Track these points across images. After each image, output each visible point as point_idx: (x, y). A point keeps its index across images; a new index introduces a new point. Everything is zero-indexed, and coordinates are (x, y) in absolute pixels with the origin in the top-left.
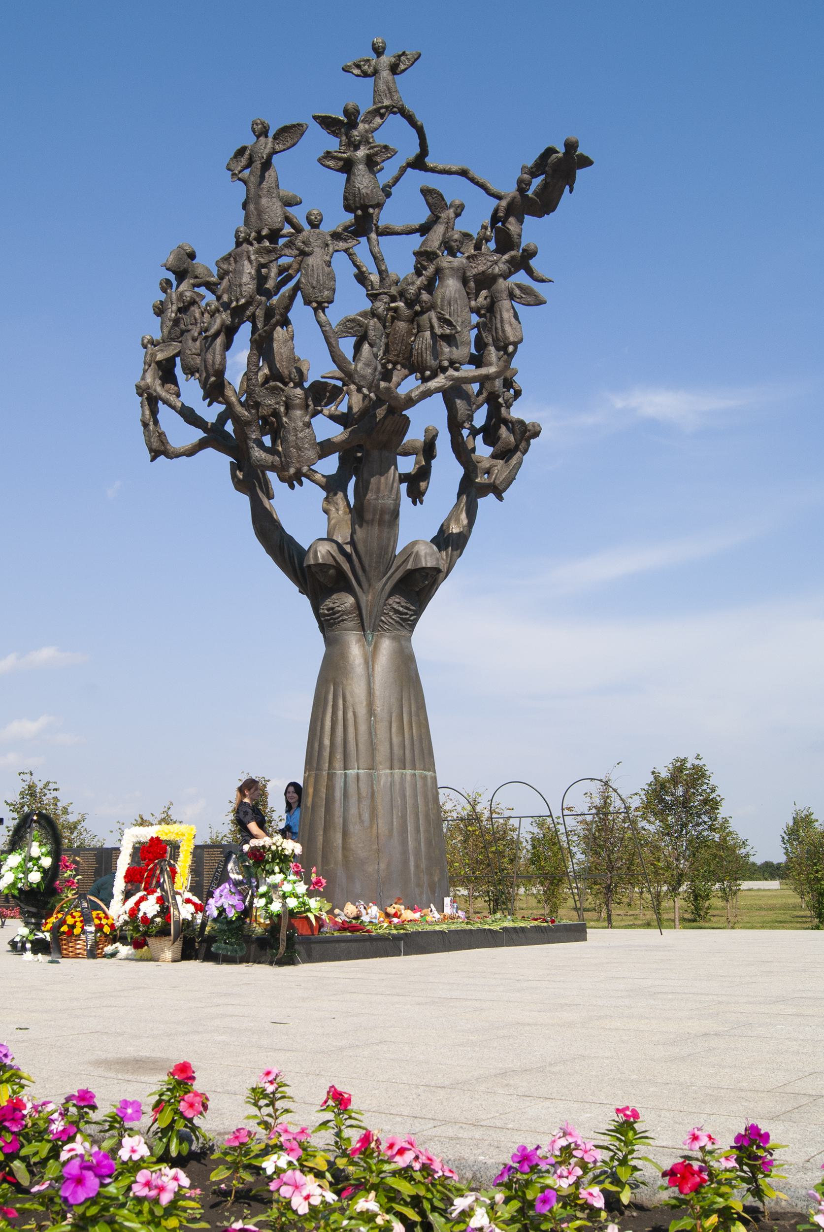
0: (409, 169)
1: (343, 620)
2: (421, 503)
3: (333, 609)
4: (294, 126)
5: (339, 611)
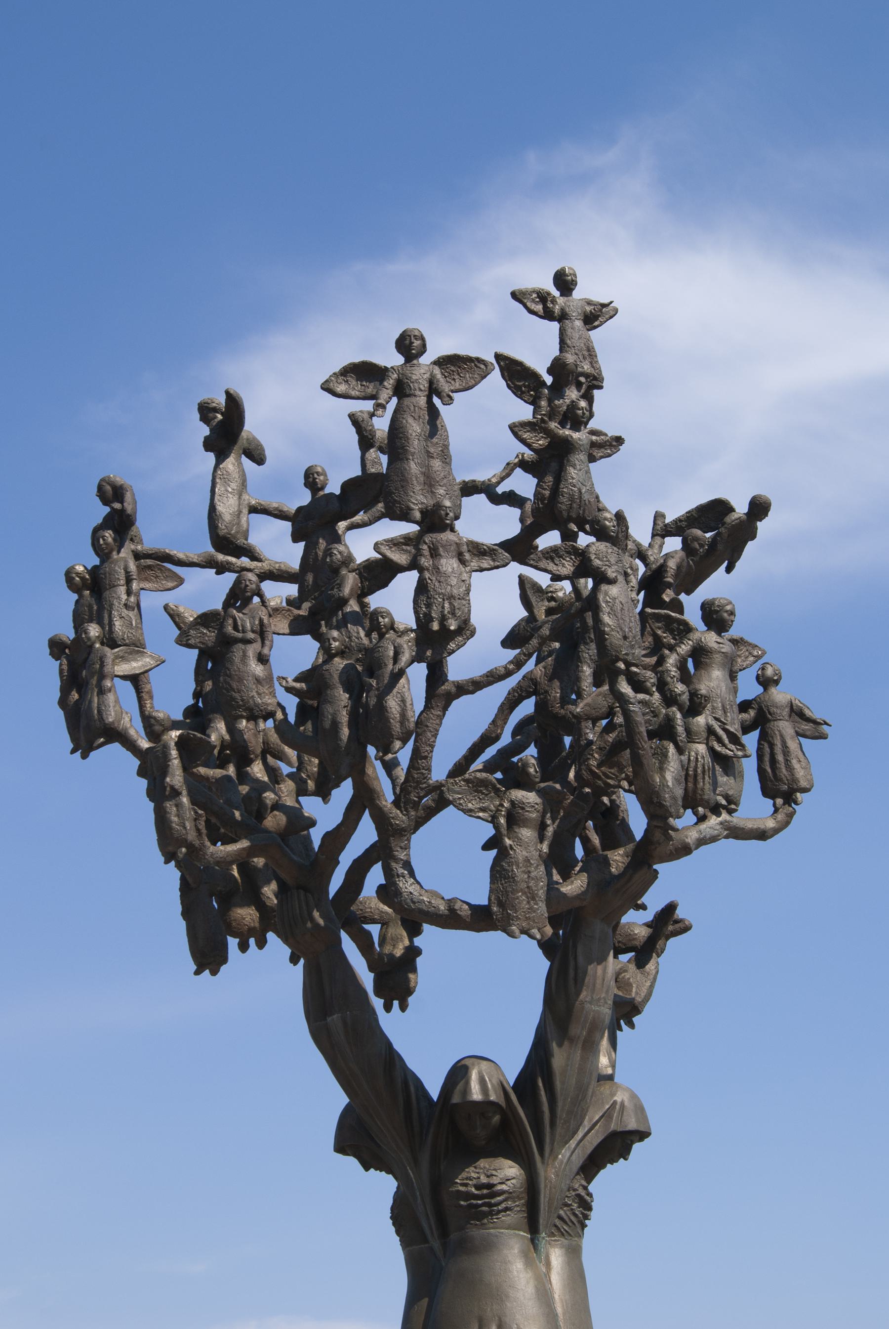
0: (518, 471)
1: (507, 1209)
2: (403, 1007)
3: (490, 1186)
4: (469, 359)
5: (502, 1192)
